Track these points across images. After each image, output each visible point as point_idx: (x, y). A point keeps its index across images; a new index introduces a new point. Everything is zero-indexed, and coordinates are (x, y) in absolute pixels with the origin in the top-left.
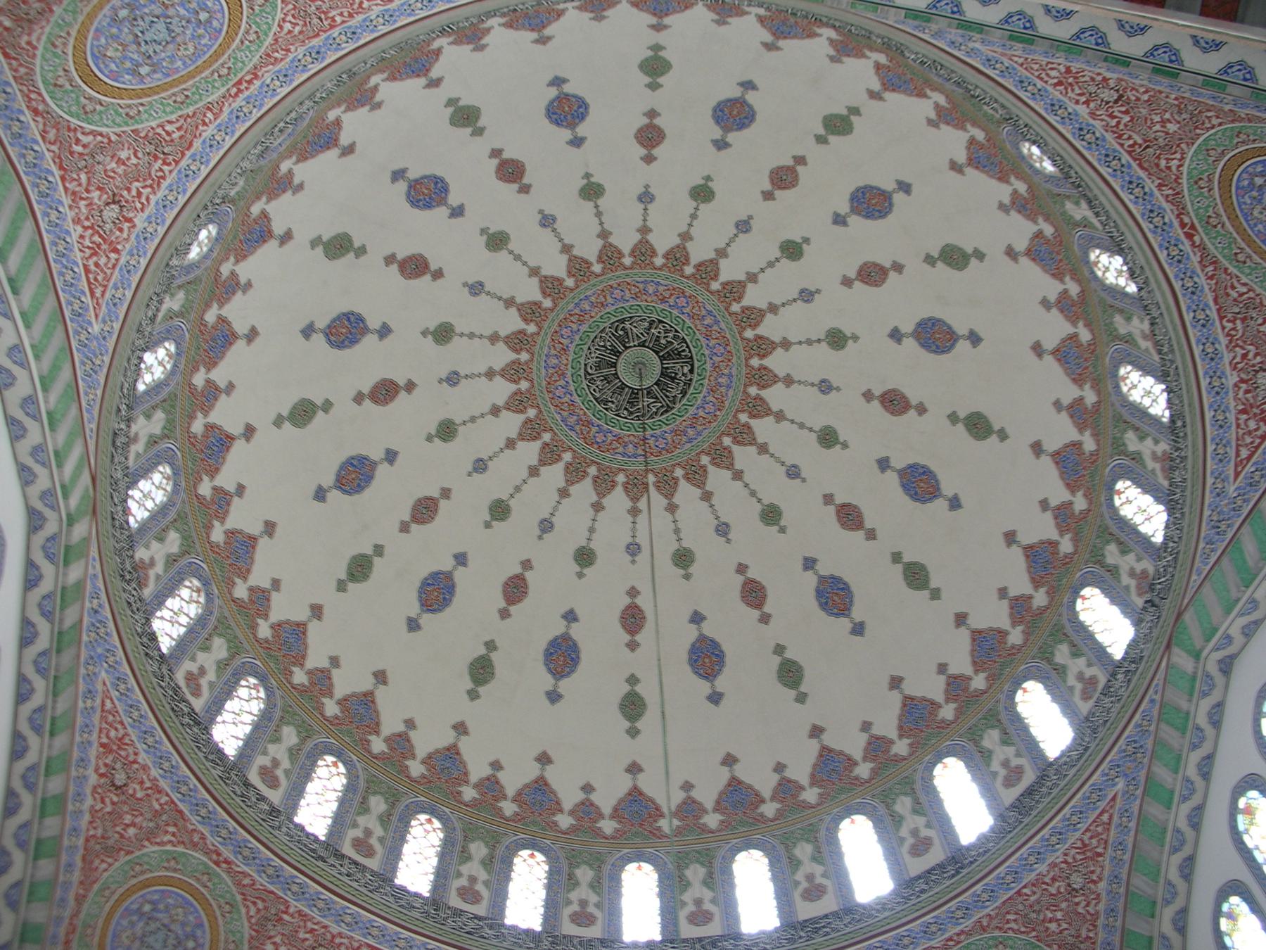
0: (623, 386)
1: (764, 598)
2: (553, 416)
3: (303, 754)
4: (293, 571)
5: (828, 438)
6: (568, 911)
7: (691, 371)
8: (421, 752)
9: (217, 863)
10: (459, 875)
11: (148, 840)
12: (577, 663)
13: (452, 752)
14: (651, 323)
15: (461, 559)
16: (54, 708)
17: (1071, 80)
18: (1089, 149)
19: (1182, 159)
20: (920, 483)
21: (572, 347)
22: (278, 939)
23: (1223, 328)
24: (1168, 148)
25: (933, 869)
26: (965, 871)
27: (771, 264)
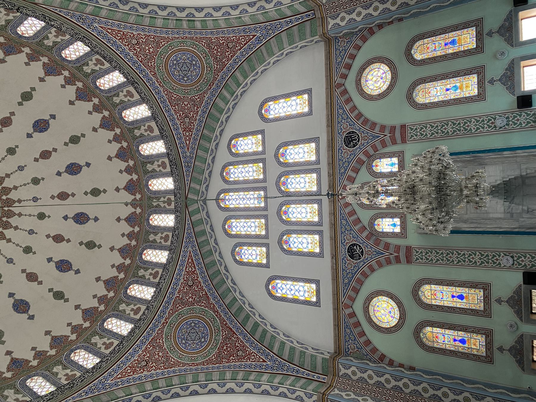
3: (128, 301)
10: (160, 242)
12: (83, 213)
13: (121, 250)
15: (50, 260)
16: (123, 397)
22: (188, 298)
25: (137, 91)
26: (136, 81)
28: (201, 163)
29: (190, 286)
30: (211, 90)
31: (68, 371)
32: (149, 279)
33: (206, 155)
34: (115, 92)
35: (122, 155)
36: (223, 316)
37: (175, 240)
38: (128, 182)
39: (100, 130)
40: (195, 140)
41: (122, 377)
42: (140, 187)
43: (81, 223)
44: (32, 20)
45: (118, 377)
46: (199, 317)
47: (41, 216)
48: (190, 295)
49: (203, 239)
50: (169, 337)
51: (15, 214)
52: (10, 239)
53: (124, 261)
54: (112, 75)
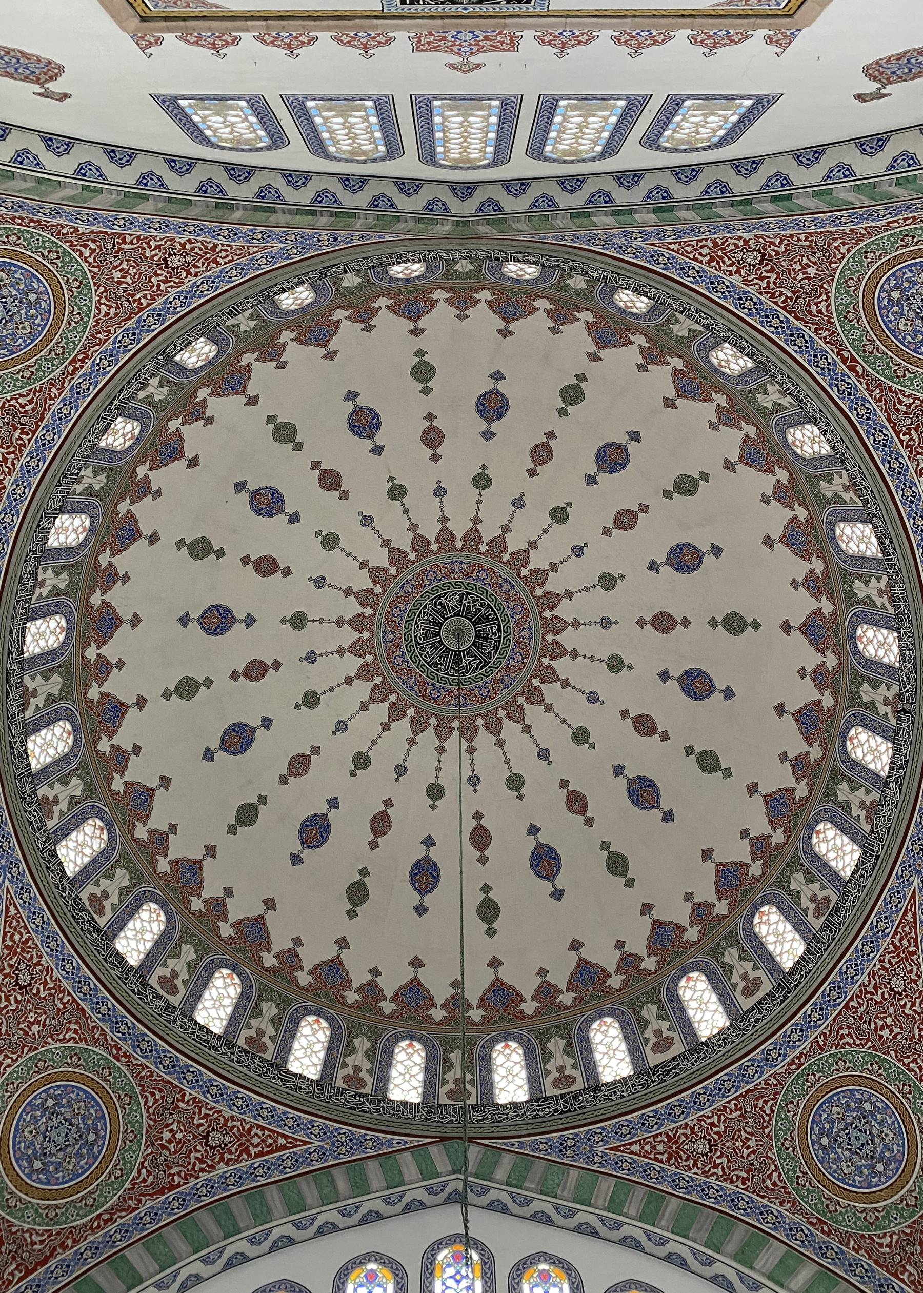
0: (448, 650)
1: (586, 804)
2: (395, 679)
3: (200, 968)
4: (189, 816)
5: (616, 664)
6: (342, 1073)
7: (499, 630)
8: (308, 965)
9: (117, 1058)
10: (345, 1065)
11: (51, 1036)
14: (462, 596)
17: (720, 253)
18: (751, 315)
19: (828, 297)
20: (696, 684)
21: (403, 623)
22: (174, 1127)
23: (901, 442)
24: (814, 293)
25: (764, 999)
26: (791, 996)
27: (545, 531)
28: (577, 1188)
29: (206, 1137)
30: (806, 1227)
31: (63, 806)
32: (249, 1026)
33: (600, 1202)
34: (751, 951)
35: (587, 975)
36: (91, 1238)
37: (348, 1097)
38: (514, 989)
39: (647, 921)
40: (646, 1171)
41: (6, 916)
42: (502, 1019)
43: (413, 875)
44: (887, 750)
45: (12, 908)
46: (107, 1159)
47: (435, 792)
48: (179, 1136)
49: (342, 1185)
50: (75, 1059)
51: (442, 740)
52: (389, 729)
53: (306, 970)
54: (793, 940)
